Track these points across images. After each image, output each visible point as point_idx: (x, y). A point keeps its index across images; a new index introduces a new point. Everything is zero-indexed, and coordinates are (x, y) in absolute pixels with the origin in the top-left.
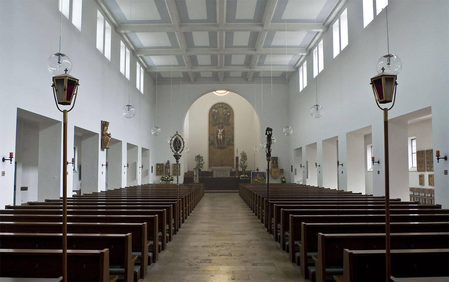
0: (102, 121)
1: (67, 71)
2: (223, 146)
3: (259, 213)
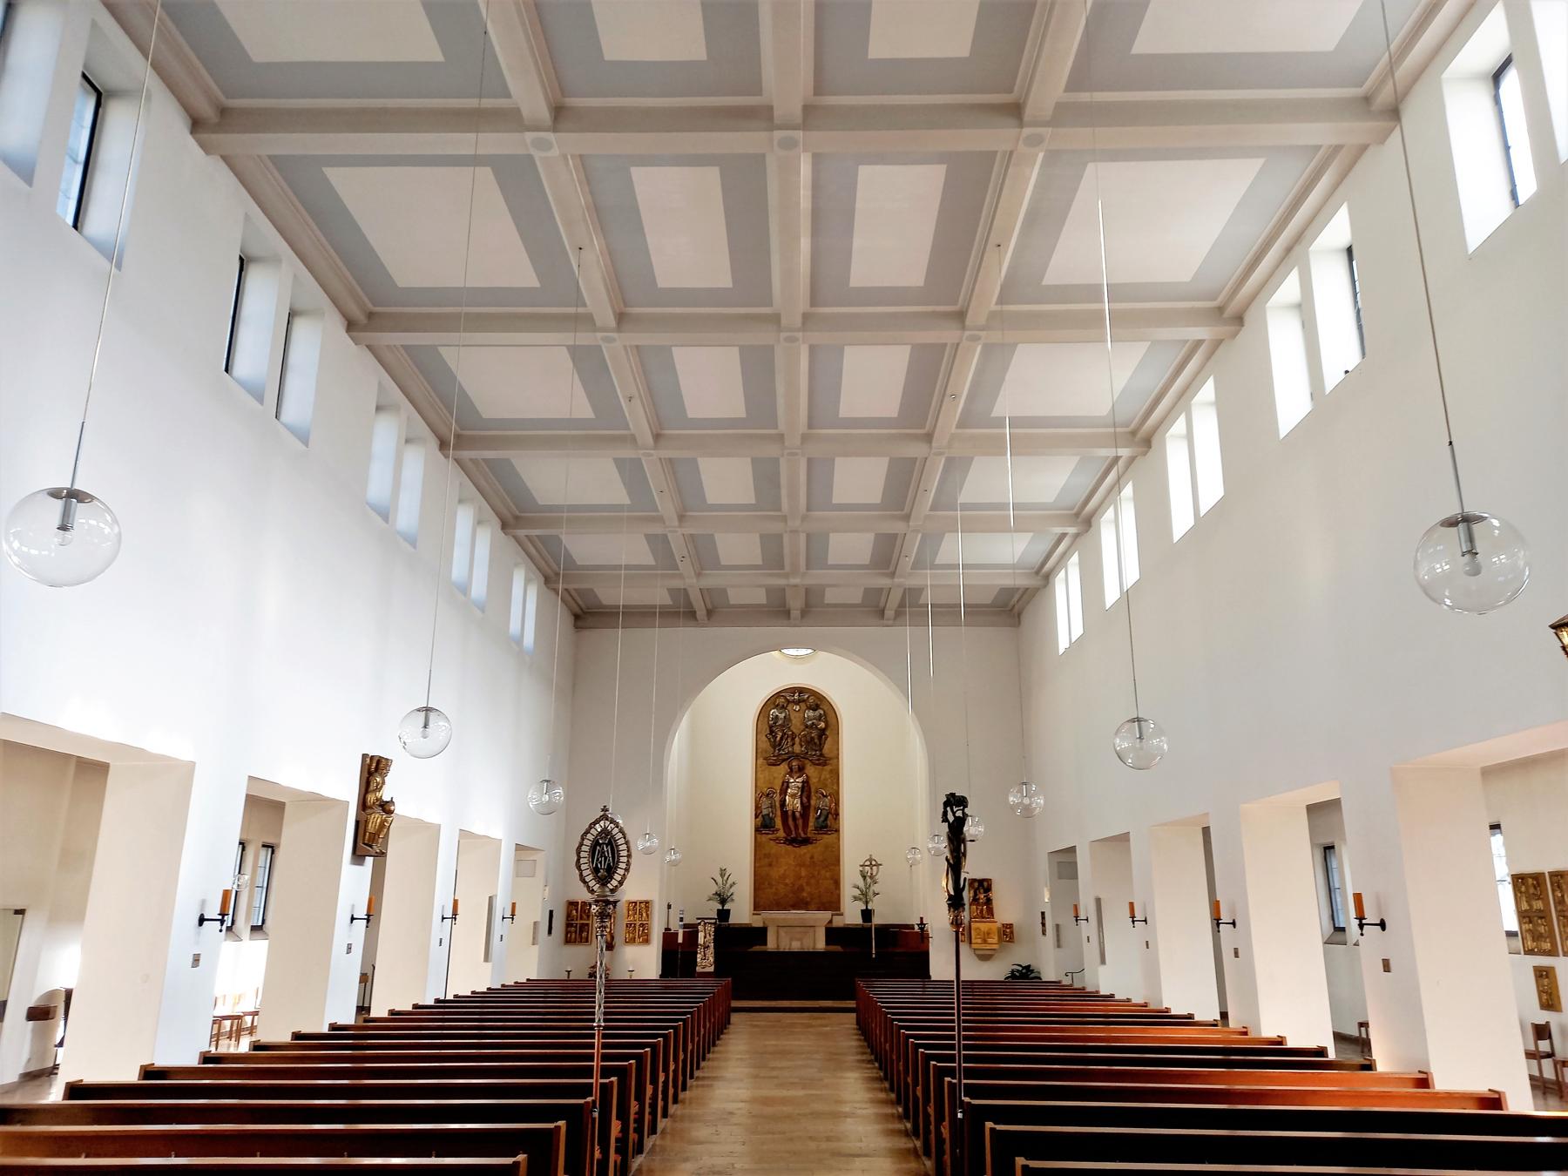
0: (365, 756)
2: (803, 835)
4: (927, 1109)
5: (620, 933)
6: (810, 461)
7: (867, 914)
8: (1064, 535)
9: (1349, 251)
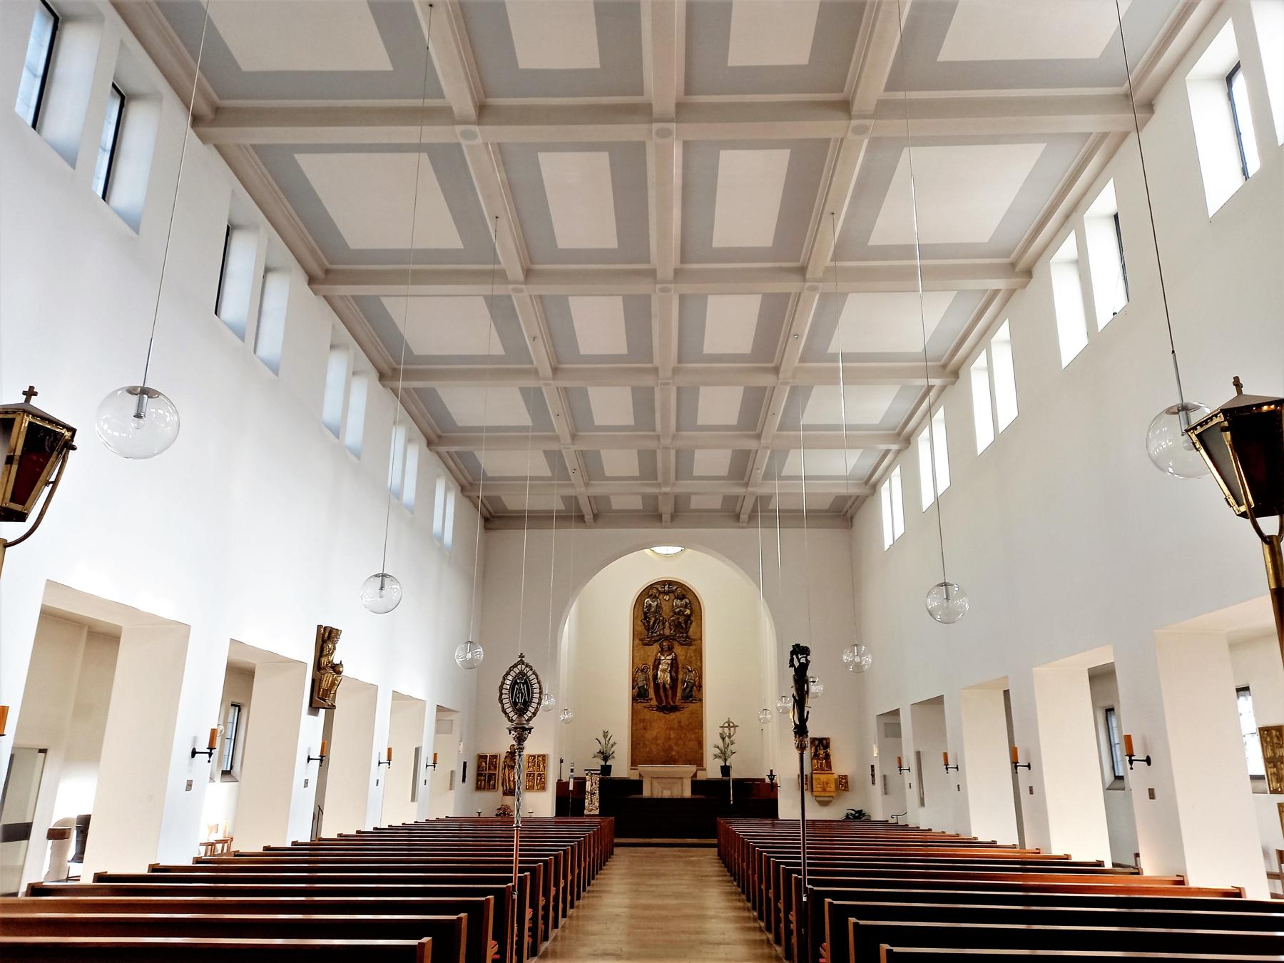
0: (319, 627)
1: (35, 394)
3: (778, 920)
4: (778, 905)
6: (679, 389)
7: (726, 770)
8: (888, 452)
9: (1116, 217)
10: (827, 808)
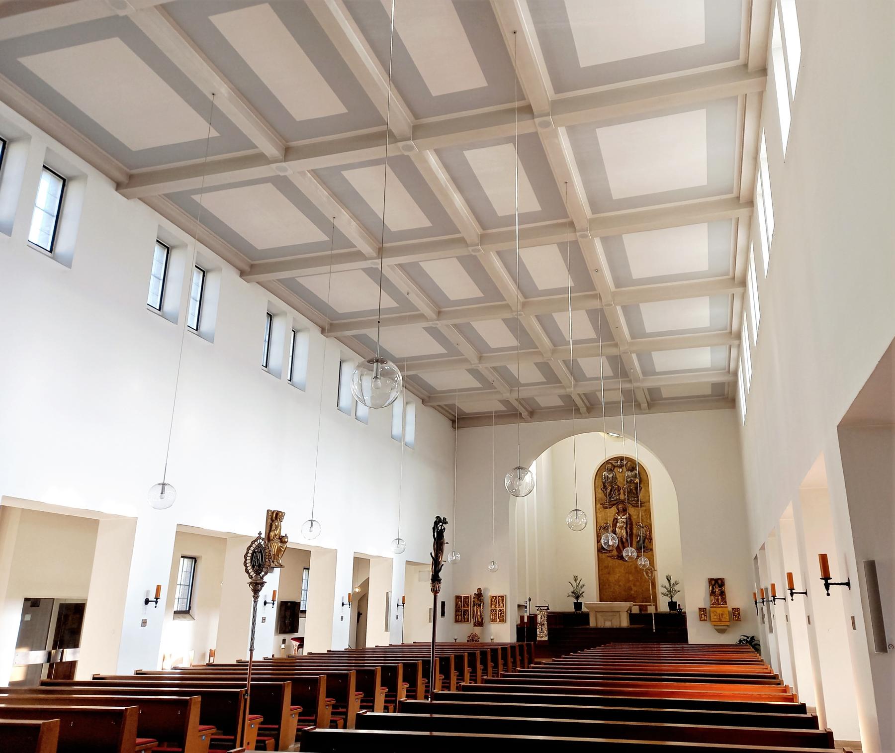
5: (487, 616)
10: (724, 634)
